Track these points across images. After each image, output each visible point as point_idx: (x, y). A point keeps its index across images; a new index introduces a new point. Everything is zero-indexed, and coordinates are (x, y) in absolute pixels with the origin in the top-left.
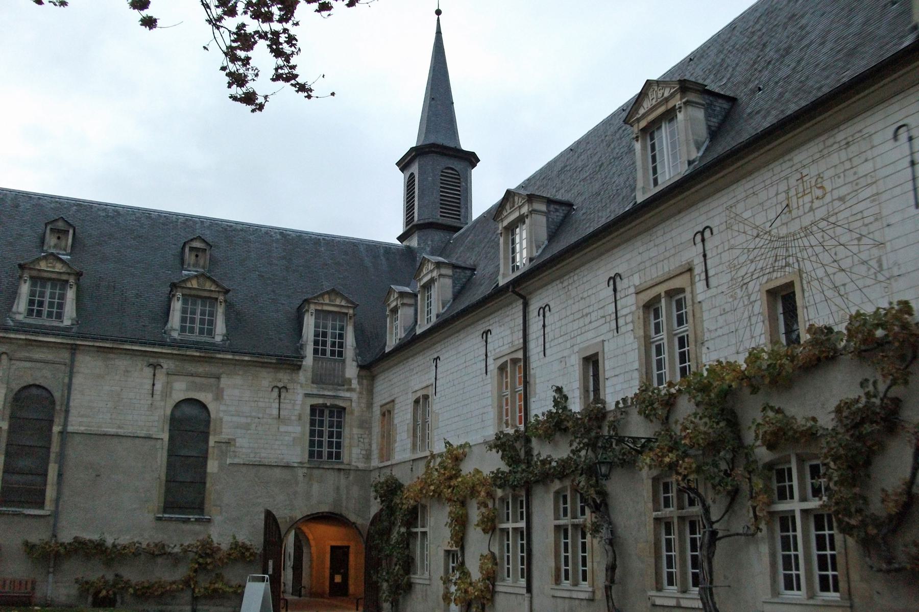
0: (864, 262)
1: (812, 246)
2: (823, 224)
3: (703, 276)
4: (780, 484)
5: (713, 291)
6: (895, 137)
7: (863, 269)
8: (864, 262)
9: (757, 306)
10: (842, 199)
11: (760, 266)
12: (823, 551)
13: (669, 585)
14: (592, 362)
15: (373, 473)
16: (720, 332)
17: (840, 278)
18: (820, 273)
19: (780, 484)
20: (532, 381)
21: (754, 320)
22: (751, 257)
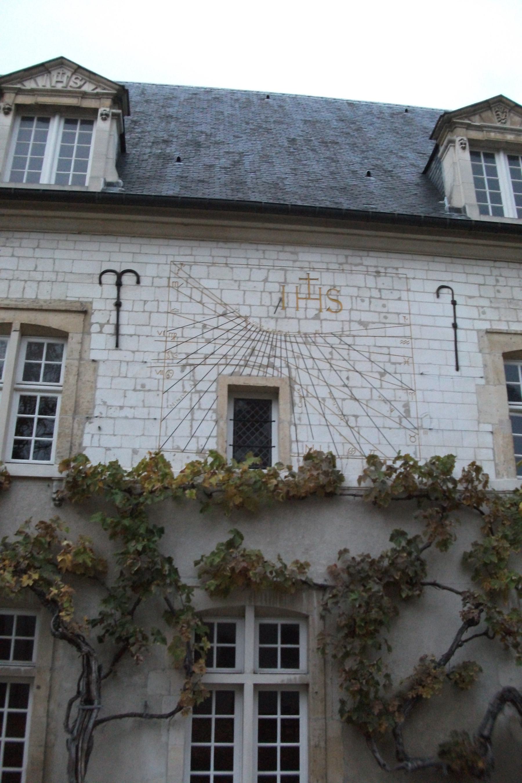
0: (386, 401)
1: (409, 301)
7: (385, 409)
8: (386, 401)
10: (364, 324)
11: (224, 350)
16: (127, 412)
17: (350, 407)
18: (323, 392)
21: (199, 415)
22: (208, 335)
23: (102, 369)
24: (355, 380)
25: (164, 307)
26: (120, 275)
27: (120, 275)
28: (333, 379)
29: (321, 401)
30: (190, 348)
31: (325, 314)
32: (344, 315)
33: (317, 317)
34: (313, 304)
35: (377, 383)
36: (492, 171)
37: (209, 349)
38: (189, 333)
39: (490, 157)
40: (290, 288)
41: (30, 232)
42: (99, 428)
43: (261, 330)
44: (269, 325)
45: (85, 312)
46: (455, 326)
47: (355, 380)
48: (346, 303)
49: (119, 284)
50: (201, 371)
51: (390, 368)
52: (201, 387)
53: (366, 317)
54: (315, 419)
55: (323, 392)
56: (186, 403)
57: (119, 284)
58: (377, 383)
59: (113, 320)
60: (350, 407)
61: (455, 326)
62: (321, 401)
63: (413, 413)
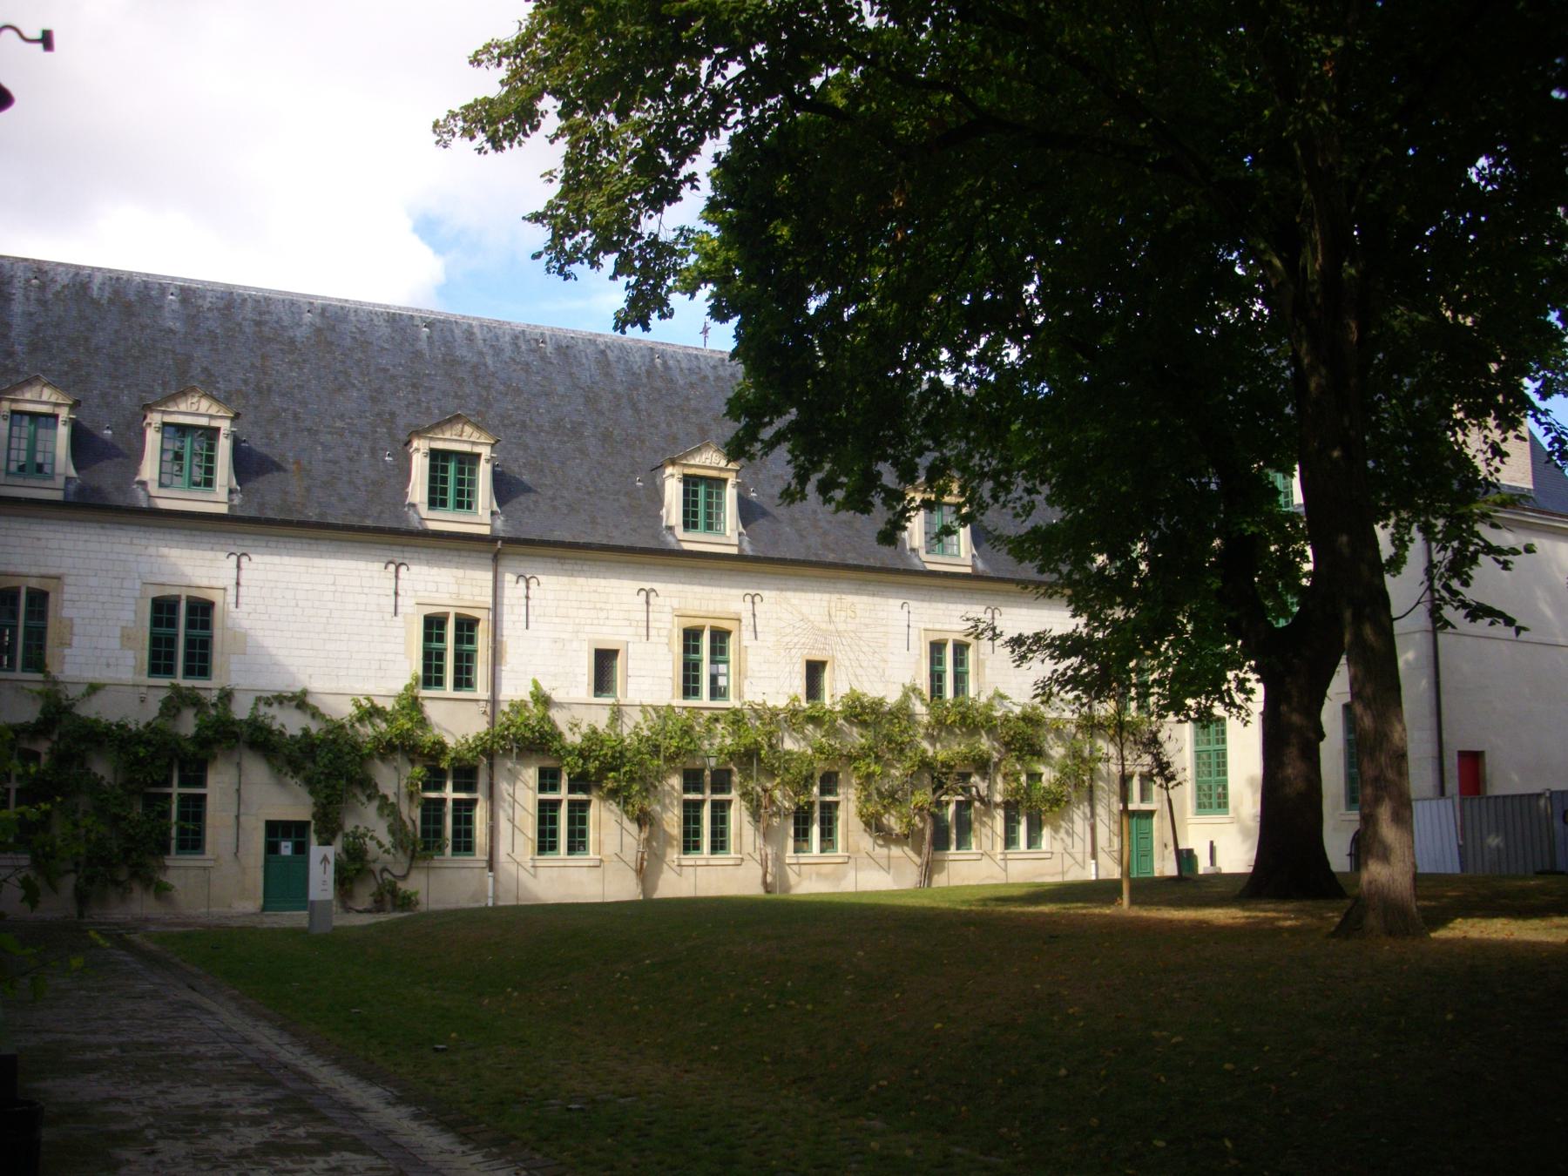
0: (875, 667)
2: (852, 635)
3: (751, 628)
4: (271, 839)
5: (759, 643)
6: (902, 607)
7: (874, 671)
8: (875, 667)
9: (797, 666)
10: (866, 625)
11: (803, 641)
12: (273, 837)
13: (1201, 807)
14: (605, 661)
15: (406, 865)
16: (762, 674)
17: (859, 671)
18: (847, 663)
19: (271, 839)
20: (501, 642)
21: (793, 675)
22: (796, 632)
23: (749, 650)
24: (862, 656)
25: (775, 616)
26: (753, 597)
27: (753, 597)
28: (852, 656)
29: (846, 668)
30: (787, 639)
31: (849, 620)
32: (857, 621)
33: (845, 622)
34: (843, 613)
35: (871, 658)
36: (695, 494)
37: (796, 640)
38: (788, 630)
39: (696, 485)
40: (833, 604)
41: (404, 546)
42: (142, 701)
43: (819, 629)
44: (824, 626)
45: (739, 620)
46: (909, 626)
47: (862, 656)
48: (858, 611)
49: (753, 603)
50: (793, 651)
51: (877, 650)
52: (794, 661)
53: (867, 621)
54: (844, 677)
55: (847, 663)
56: (788, 669)
57: (753, 603)
58: (871, 658)
59: (752, 623)
60: (859, 671)
61: (909, 626)
62: (846, 668)
63: (886, 674)
